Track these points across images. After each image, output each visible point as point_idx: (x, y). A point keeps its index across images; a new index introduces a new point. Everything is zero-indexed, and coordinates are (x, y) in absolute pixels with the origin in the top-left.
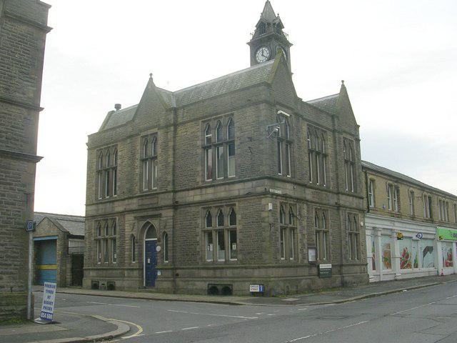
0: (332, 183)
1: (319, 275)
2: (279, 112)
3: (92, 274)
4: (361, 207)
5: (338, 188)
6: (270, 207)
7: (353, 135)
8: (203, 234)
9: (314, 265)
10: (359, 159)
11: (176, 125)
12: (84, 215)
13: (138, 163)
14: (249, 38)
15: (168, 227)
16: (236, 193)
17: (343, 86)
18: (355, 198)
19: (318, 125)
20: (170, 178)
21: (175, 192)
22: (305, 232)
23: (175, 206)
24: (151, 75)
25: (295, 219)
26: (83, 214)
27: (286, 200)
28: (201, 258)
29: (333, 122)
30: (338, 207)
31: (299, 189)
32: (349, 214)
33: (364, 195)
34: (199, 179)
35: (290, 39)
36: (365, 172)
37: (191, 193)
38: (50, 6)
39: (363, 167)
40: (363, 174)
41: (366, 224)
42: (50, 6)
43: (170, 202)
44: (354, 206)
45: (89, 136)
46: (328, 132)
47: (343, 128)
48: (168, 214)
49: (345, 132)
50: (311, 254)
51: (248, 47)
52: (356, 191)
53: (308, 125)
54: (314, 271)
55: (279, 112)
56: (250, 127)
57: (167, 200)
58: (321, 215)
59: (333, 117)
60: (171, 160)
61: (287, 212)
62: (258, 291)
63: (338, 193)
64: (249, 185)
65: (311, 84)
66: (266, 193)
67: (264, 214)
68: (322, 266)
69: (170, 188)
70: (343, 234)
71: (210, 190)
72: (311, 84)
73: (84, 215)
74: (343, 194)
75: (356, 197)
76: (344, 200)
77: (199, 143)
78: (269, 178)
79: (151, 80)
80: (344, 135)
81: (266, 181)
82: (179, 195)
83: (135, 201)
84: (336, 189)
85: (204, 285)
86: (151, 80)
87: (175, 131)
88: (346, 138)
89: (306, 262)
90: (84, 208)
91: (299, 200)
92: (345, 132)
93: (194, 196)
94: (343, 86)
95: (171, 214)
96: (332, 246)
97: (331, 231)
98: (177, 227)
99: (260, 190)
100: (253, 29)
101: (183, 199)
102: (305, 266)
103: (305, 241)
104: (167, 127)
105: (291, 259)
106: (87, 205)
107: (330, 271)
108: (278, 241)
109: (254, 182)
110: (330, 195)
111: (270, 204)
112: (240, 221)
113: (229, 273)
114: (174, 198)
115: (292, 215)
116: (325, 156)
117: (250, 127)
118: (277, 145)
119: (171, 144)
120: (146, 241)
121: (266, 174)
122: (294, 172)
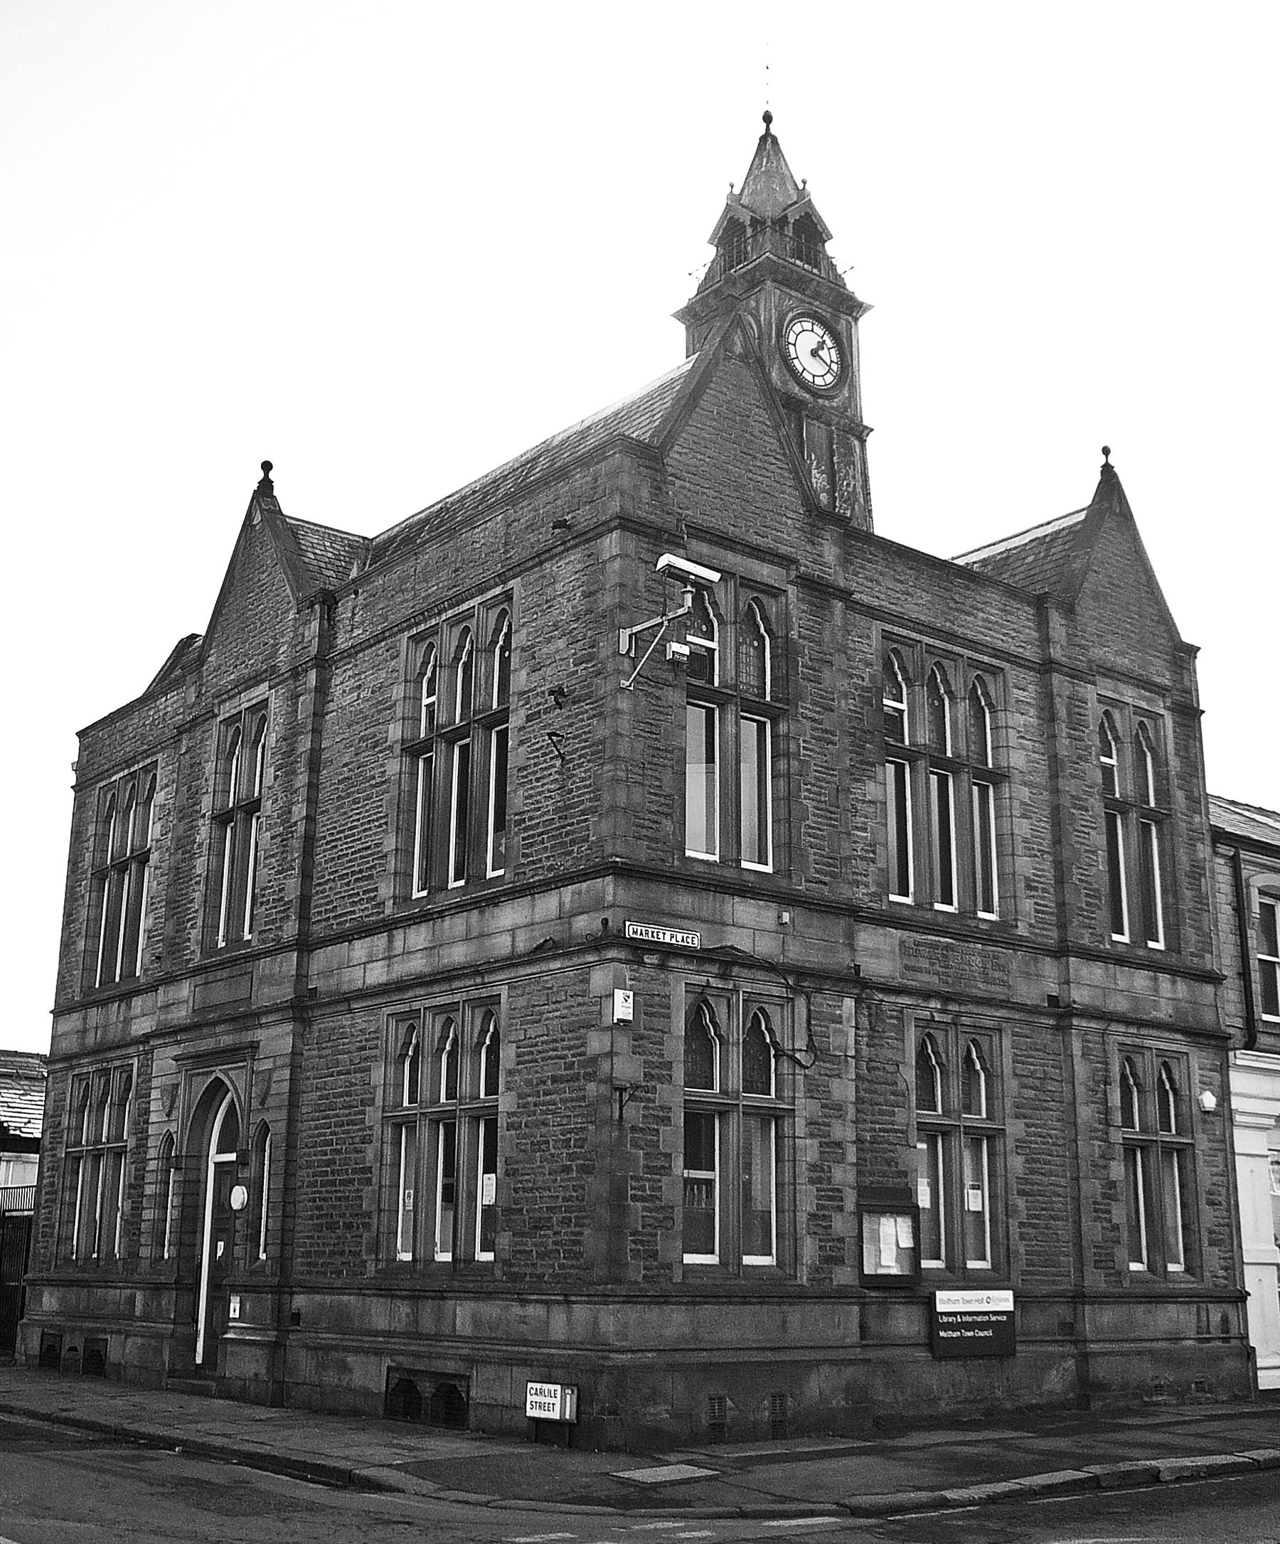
0: (1027, 905)
1: (932, 1343)
2: (663, 561)
3: (49, 1301)
4: (1208, 1017)
5: (1062, 926)
6: (623, 1007)
7: (1161, 690)
8: (389, 1132)
9: (912, 1288)
10: (1198, 799)
11: (324, 662)
12: (46, 1051)
13: (204, 832)
14: (687, 291)
15: (271, 1102)
16: (501, 945)
17: (1107, 470)
18: (1164, 978)
19: (951, 637)
20: (292, 886)
21: (305, 945)
22: (844, 1131)
23: (303, 1007)
24: (267, 466)
25: (786, 1067)
26: (43, 1047)
27: (723, 976)
28: (375, 1247)
29: (1042, 622)
30: (1061, 1012)
31: (817, 927)
32: (1130, 1054)
33: (1226, 963)
34: (386, 890)
35: (856, 285)
36: (1235, 863)
37: (359, 949)
38: (1198, 649)
39: (1219, 836)
40: (1223, 871)
41: (1236, 1103)
42: (1198, 649)
43: (286, 993)
44: (1163, 1012)
45: (81, 734)
46: (1012, 673)
47: (1098, 653)
48: (276, 1039)
49: (1109, 672)
50: (888, 1246)
51: (680, 330)
52: (1174, 943)
53: (887, 636)
54: (905, 1322)
55: (663, 561)
56: (561, 643)
57: (274, 980)
58: (952, 1048)
59: (1040, 604)
60: (300, 811)
61: (737, 1033)
62: (555, 1415)
63: (1061, 952)
64: (548, 905)
65: (949, 477)
66: (607, 939)
67: (596, 1043)
68: (948, 1301)
69: (290, 929)
70: (1089, 1149)
71: (419, 937)
72: (949, 477)
73: (46, 1051)
74: (1089, 955)
75: (1174, 972)
76: (1088, 983)
77: (395, 732)
78: (625, 872)
79: (265, 489)
80: (1106, 688)
81: (608, 887)
82: (321, 959)
83: (184, 990)
84: (1054, 934)
85: (370, 1375)
86: (265, 489)
87: (322, 690)
88: (1115, 703)
89: (843, 1276)
90: (47, 1022)
91: (803, 979)
92: (1109, 672)
93: (365, 965)
94: (1107, 470)
95: (287, 1044)
96: (1021, 1203)
97: (1015, 1128)
98: (309, 1098)
99: (584, 924)
100: (701, 255)
101: (333, 981)
102: (842, 1295)
103: (844, 1175)
104: (296, 673)
105: (1172, 1267)
106: (58, 1013)
107: (1003, 1327)
108: (666, 1170)
109: (568, 893)
110: (1016, 960)
111: (619, 994)
112: (510, 1073)
113: (462, 1315)
114: (301, 976)
115: (760, 1052)
116: (998, 777)
117: (561, 643)
118: (1102, 823)
119: (305, 743)
120: (218, 1165)
121: (618, 851)
122: (787, 848)
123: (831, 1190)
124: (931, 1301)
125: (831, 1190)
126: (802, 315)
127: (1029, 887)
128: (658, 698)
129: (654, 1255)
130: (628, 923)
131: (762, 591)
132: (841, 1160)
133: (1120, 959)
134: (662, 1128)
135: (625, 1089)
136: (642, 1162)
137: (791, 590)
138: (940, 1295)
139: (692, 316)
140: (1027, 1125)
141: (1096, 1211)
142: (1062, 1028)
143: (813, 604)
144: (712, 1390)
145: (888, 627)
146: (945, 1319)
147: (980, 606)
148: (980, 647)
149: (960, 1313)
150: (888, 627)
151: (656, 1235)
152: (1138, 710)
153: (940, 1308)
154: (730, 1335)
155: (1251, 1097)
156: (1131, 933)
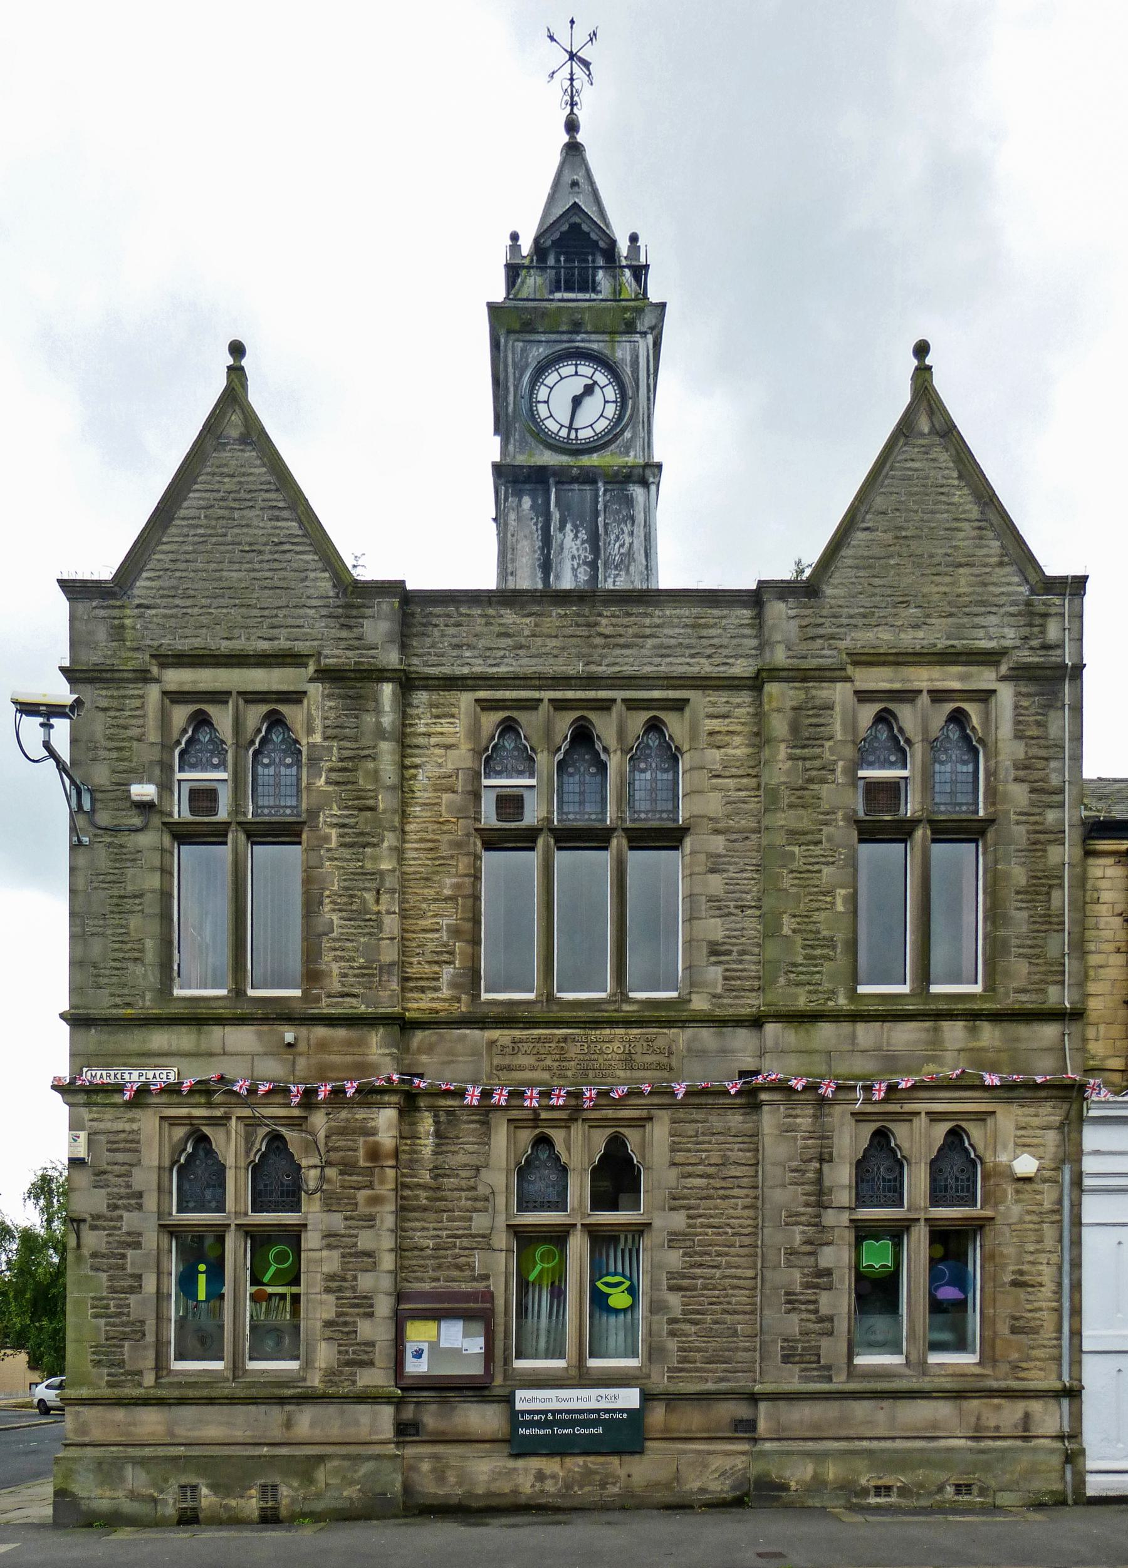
103: (378, 1283)
123: (355, 1298)
124: (510, 1400)
125: (355, 1298)
126: (542, 369)
127: (714, 952)
128: (122, 846)
129: (121, 1364)
130: (85, 1069)
131: (278, 701)
132: (374, 1267)
133: (890, 1013)
134: (130, 1253)
135: (84, 1221)
136: (106, 1284)
137: (315, 690)
138: (520, 1394)
139: (497, 431)
140: (689, 1217)
141: (789, 1302)
142: (755, 1107)
143: (340, 697)
144: (184, 1480)
145: (482, 694)
146: (527, 1417)
147: (648, 631)
148: (828, 674)
149: (553, 1412)
150: (482, 694)
151: (123, 1346)
152: (938, 696)
153: (519, 1406)
154: (213, 1432)
155: (211, 1401)
156: (913, 981)
